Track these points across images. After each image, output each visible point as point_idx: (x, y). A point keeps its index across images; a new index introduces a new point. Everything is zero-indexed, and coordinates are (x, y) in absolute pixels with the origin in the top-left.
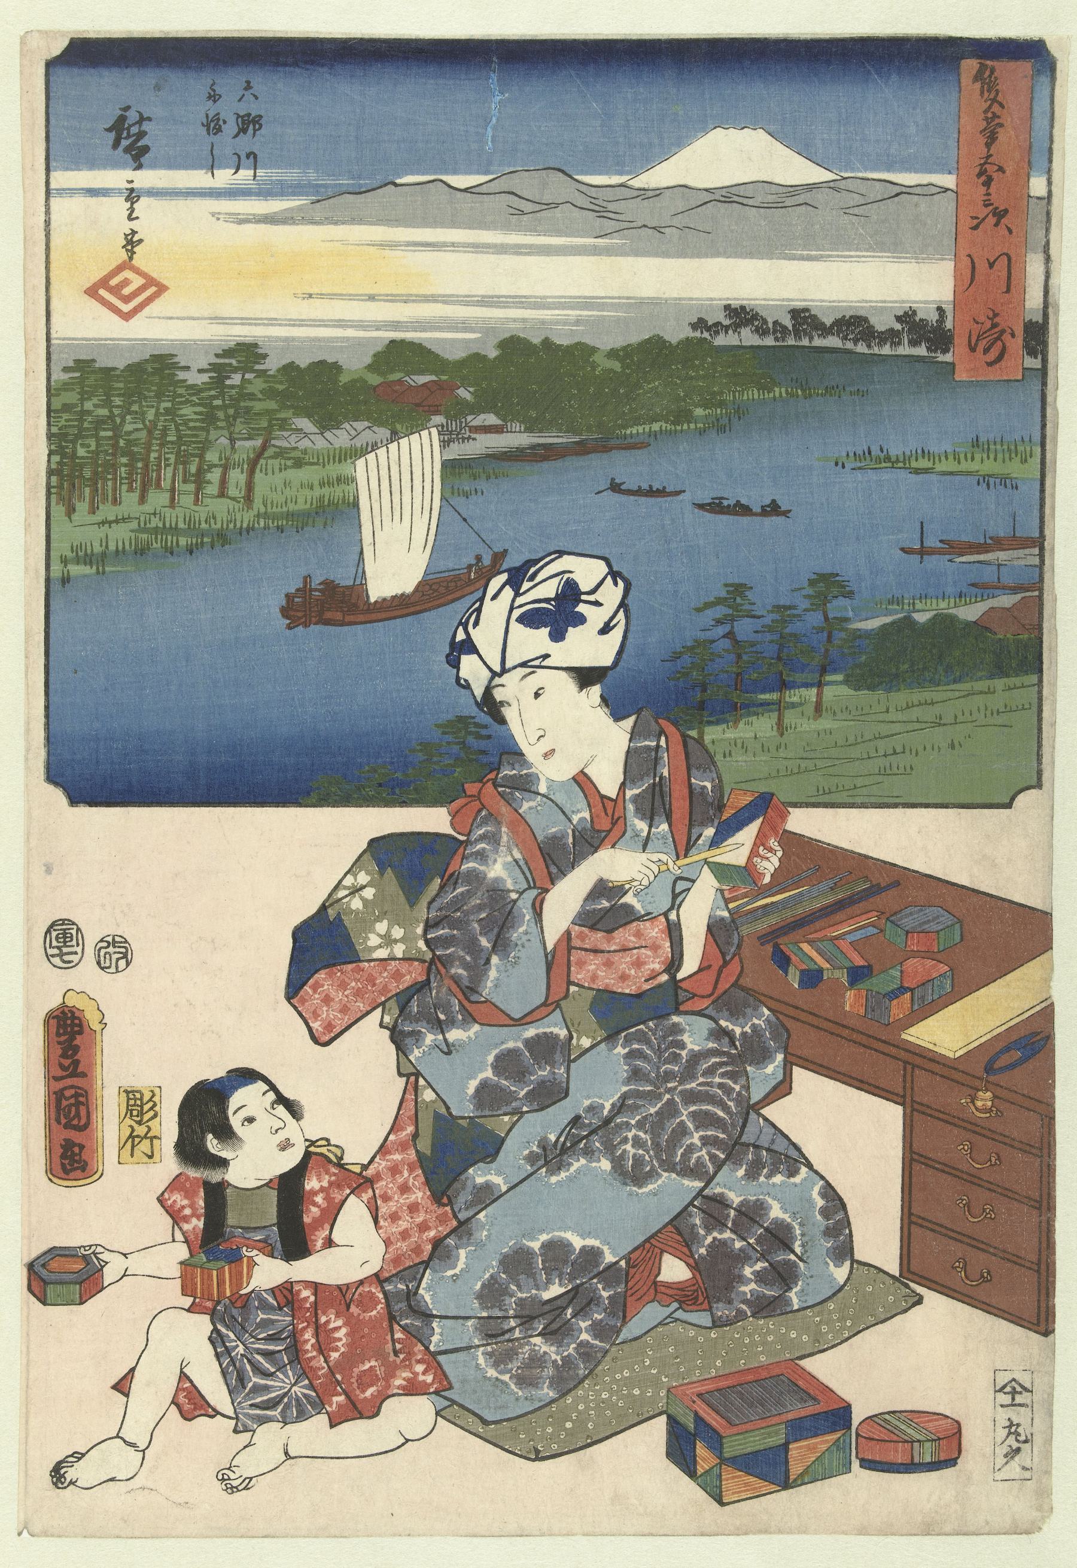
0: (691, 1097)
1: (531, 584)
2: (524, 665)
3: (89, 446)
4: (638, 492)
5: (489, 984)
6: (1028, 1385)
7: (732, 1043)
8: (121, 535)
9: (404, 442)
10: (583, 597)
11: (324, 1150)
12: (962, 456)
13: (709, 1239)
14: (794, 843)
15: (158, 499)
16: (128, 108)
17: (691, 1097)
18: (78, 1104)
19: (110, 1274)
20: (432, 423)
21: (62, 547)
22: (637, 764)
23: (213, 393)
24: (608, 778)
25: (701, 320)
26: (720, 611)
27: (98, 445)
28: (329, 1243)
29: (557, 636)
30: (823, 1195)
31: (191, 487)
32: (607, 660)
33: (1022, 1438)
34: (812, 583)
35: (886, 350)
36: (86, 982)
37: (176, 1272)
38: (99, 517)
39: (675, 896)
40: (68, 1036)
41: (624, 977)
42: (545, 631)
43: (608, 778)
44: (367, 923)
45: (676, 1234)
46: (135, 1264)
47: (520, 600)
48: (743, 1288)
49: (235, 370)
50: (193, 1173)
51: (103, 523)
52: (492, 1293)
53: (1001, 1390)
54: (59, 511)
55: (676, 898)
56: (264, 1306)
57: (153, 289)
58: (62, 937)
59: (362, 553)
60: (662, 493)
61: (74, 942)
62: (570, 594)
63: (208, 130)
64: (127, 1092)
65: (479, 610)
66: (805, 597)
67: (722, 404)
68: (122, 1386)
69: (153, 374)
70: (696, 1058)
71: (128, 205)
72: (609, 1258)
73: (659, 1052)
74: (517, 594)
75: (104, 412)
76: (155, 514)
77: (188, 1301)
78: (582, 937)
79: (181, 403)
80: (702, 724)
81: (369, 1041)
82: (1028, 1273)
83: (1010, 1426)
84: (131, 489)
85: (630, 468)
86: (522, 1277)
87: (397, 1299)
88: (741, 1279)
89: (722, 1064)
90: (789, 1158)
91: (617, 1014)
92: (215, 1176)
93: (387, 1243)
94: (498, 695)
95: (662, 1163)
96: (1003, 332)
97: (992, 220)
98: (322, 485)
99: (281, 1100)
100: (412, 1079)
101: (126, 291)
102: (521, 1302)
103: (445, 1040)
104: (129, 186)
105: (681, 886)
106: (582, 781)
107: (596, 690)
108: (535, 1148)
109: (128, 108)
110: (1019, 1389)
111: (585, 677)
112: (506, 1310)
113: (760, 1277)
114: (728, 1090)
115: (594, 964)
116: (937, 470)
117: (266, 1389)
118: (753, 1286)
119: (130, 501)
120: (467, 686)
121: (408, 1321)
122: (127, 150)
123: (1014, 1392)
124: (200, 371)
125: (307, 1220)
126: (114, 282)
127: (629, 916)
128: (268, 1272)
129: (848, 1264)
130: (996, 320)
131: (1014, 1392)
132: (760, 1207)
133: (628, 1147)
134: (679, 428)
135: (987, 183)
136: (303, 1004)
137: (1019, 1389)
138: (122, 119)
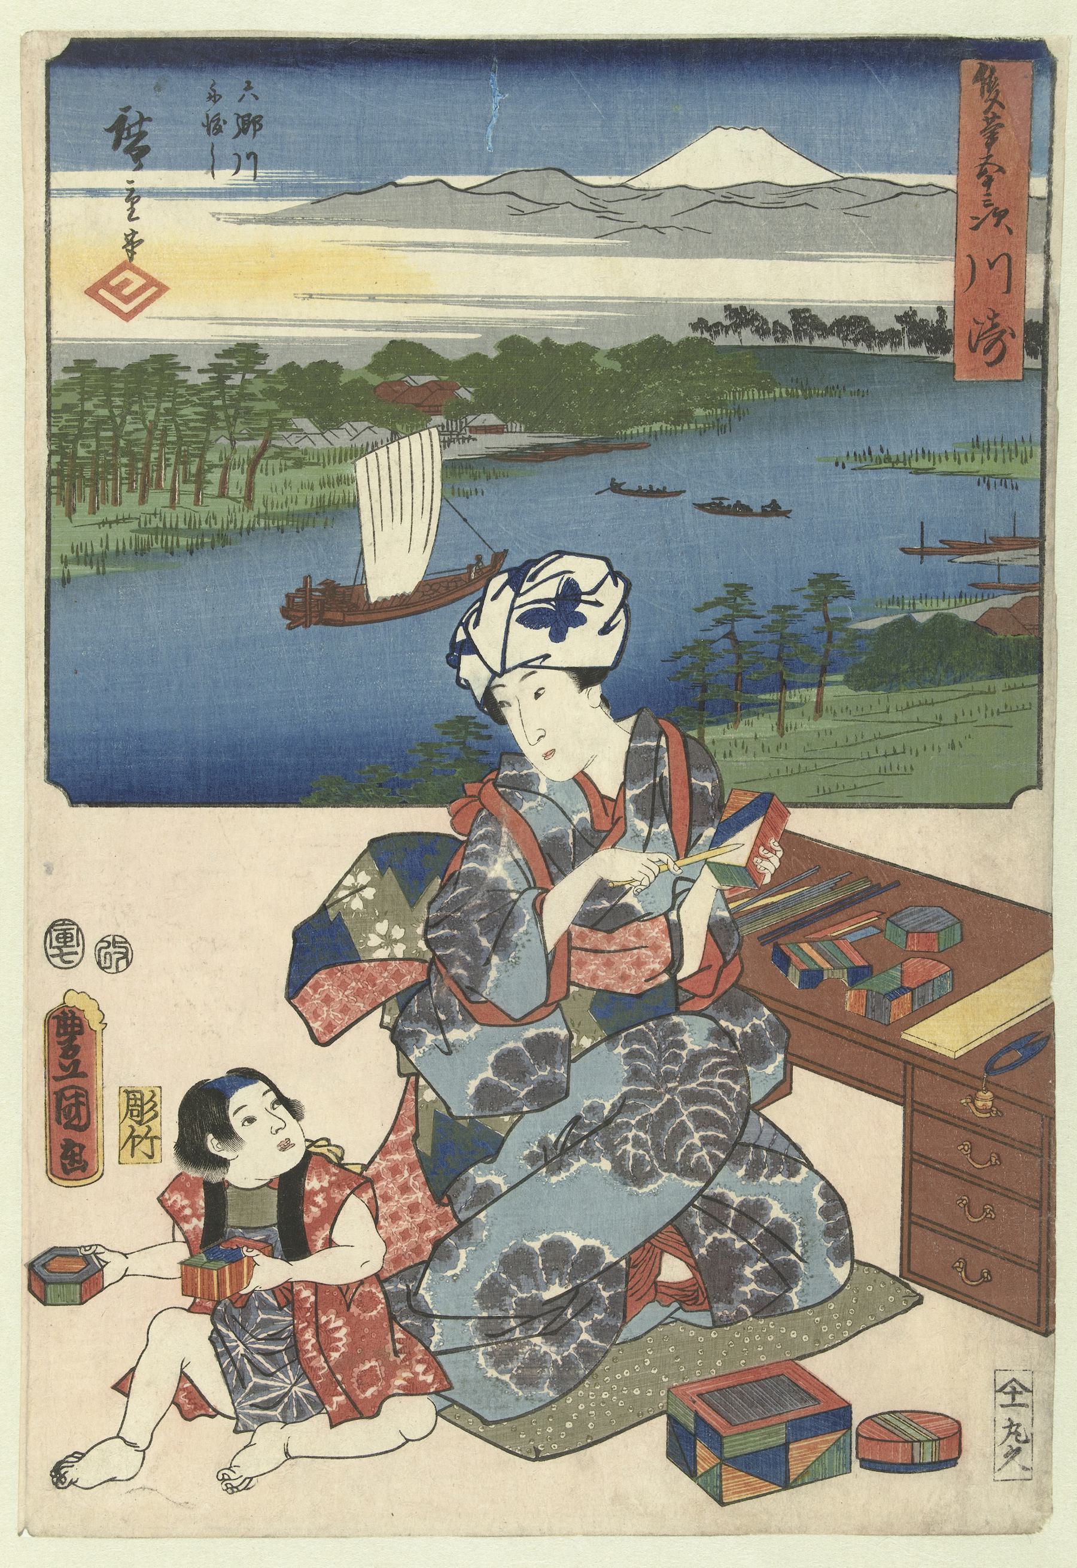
0: (691, 1098)
1: (532, 584)
2: (524, 665)
4: (639, 493)
6: (1028, 1385)
8: (121, 535)
9: (404, 442)
10: (584, 597)
11: (324, 1150)
12: (962, 456)
13: (710, 1239)
14: (794, 843)
15: (158, 499)
17: (691, 1098)
18: (78, 1104)
19: (110, 1274)
21: (62, 547)
22: (637, 764)
23: (213, 393)
24: (608, 779)
26: (721, 611)
28: (330, 1243)
29: (558, 636)
30: (823, 1195)
31: (192, 487)
33: (1023, 1438)
34: (812, 583)
35: (887, 350)
36: (86, 982)
38: (99, 517)
39: (675, 896)
40: (69, 1036)
41: (624, 978)
42: (545, 632)
43: (608, 779)
44: (367, 923)
45: (677, 1234)
46: (135, 1264)
47: (520, 601)
48: (744, 1289)
49: (236, 370)
50: (193, 1173)
51: (103, 523)
52: (492, 1293)
53: (1001, 1390)
54: (59, 511)
55: (677, 899)
56: (265, 1306)
57: (153, 290)
58: (62, 937)
59: (362, 553)
60: (662, 493)
61: (74, 942)
62: (570, 594)
63: (208, 130)
64: (127, 1092)
65: (479, 611)
66: (805, 597)
67: (722, 404)
68: (123, 1386)
70: (696, 1058)
72: (609, 1258)
73: (659, 1052)
74: (518, 594)
75: (104, 412)
76: (155, 514)
77: (188, 1301)
78: (582, 937)
79: (182, 403)
80: (702, 724)
81: (370, 1041)
83: (1010, 1427)
84: (131, 490)
85: (630, 469)
86: (523, 1277)
88: (742, 1279)
89: (722, 1064)
90: (790, 1158)
91: (617, 1014)
92: (215, 1177)
93: (388, 1243)
94: (499, 695)
95: (662, 1163)
96: (1003, 332)
100: (413, 1079)
101: (127, 291)
102: (521, 1302)
103: (446, 1040)
104: (130, 186)
105: (681, 886)
106: (583, 781)
107: (596, 691)
108: (535, 1148)
110: (1019, 1389)
111: (585, 677)
112: (506, 1310)
113: (760, 1277)
114: (728, 1091)
115: (594, 964)
117: (267, 1389)
118: (753, 1286)
119: (130, 501)
122: (127, 150)
123: (1014, 1392)
124: (200, 371)
125: (307, 1220)
126: (114, 282)
127: (629, 916)
128: (268, 1272)
129: (848, 1264)
131: (1014, 1392)
132: (761, 1207)
133: (629, 1147)
135: (988, 184)
137: (1019, 1389)
138: (122, 119)
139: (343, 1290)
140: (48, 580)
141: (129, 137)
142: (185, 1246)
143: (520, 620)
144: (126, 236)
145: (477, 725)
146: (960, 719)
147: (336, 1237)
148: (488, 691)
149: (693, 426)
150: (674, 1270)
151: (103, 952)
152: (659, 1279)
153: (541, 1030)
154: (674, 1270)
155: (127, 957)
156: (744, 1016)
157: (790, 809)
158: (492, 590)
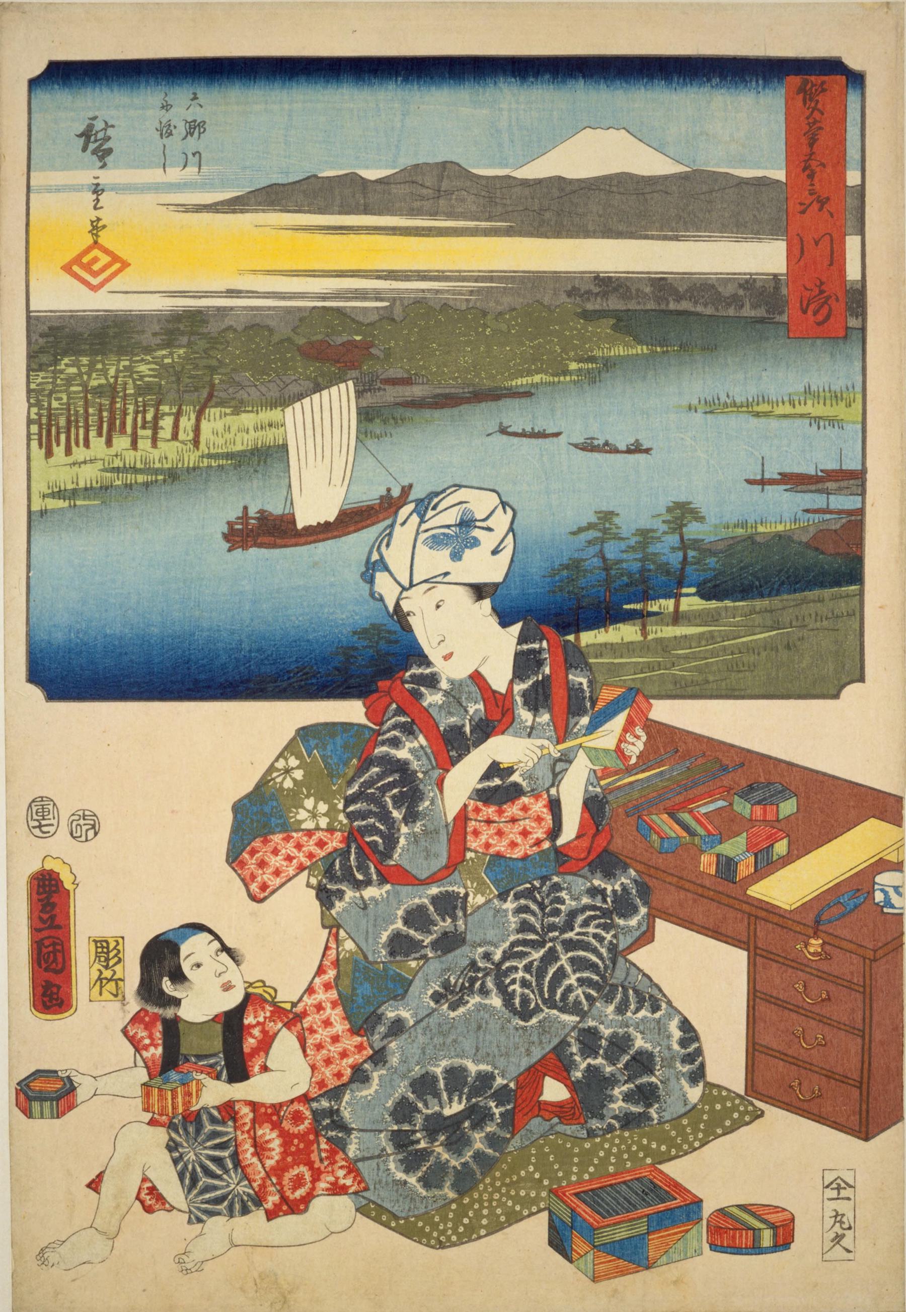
0: (569, 945)
1: (434, 512)
2: (426, 581)
3: (61, 399)
4: (523, 435)
5: (399, 851)
6: (851, 1183)
7: (604, 901)
8: (89, 475)
9: (325, 393)
10: (478, 524)
11: (260, 991)
12: (797, 403)
13: (583, 1066)
14: (665, 739)
15: (122, 443)
16: (95, 118)
17: (569, 945)
18: (54, 952)
19: (82, 1094)
20: (349, 376)
21: (40, 486)
22: (525, 663)
23: (164, 352)
24: (500, 677)
25: (574, 288)
26: (592, 534)
27: (69, 398)
28: (265, 1069)
29: (456, 556)
30: (681, 1028)
31: (149, 432)
32: (498, 578)
33: (846, 1226)
34: (669, 510)
35: (731, 312)
36: (60, 851)
37: (138, 1091)
38: (70, 460)
39: (555, 775)
40: (48, 897)
41: (513, 844)
42: (447, 552)
43: (500, 677)
44: (295, 798)
45: (557, 1063)
46: (101, 1084)
47: (424, 526)
48: (612, 1106)
49: (183, 334)
50: (153, 1009)
51: (74, 464)
52: (403, 1111)
53: (827, 1187)
54: (38, 453)
55: (556, 777)
56: (213, 1120)
57: (117, 266)
58: (40, 814)
59: (290, 486)
60: (542, 435)
61: (51, 816)
62: (467, 523)
63: (161, 135)
64: (96, 942)
65: (390, 535)
66: (664, 522)
67: (592, 359)
68: (95, 1185)
69: (114, 337)
70: (573, 914)
71: (95, 196)
72: (499, 1081)
73: (542, 906)
74: (422, 521)
75: (73, 370)
76: (116, 456)
77: (147, 1116)
78: (477, 810)
79: (137, 361)
80: (578, 631)
81: (298, 900)
82: (854, 1089)
83: (836, 1217)
84: (100, 434)
85: (517, 415)
86: (429, 1097)
87: (317, 1126)
88: (611, 1099)
89: (594, 918)
90: (651, 997)
91: (505, 874)
92: (169, 1013)
93: (313, 1068)
94: (406, 606)
95: (545, 1002)
96: (829, 297)
97: (816, 206)
98: (256, 429)
99: (225, 949)
100: (334, 930)
101: (96, 267)
102: (427, 1118)
103: (362, 897)
104: (96, 181)
105: (559, 767)
106: (477, 677)
107: (487, 603)
108: (437, 988)
109: (95, 118)
110: (843, 1185)
111: (479, 591)
112: (415, 1125)
113: (627, 1097)
114: (601, 939)
115: (487, 833)
116: (777, 413)
117: (215, 1188)
118: (620, 1103)
119: (98, 443)
120: (381, 599)
121: (334, 1133)
122: (94, 152)
123: (839, 1188)
124: (155, 334)
125: (247, 1049)
126: (85, 260)
127: (515, 792)
128: (214, 1092)
129: (701, 1084)
130: (823, 287)
131: (839, 1188)
132: (628, 1039)
133: (516, 987)
134: (556, 379)
135: (811, 176)
136: (242, 868)
137: (843, 1185)
138: (90, 127)
139: (277, 1108)
140: (29, 512)
141: (96, 141)
142: (145, 1070)
143: (425, 542)
144: (92, 222)
145: (389, 632)
146: (794, 623)
147: (269, 1064)
148: (397, 605)
149: (568, 378)
150: (554, 1091)
151: (75, 823)
152: (542, 1098)
153: (442, 889)
154: (554, 1091)
155: (95, 828)
156: (614, 876)
157: (652, 701)
158: (400, 519)
